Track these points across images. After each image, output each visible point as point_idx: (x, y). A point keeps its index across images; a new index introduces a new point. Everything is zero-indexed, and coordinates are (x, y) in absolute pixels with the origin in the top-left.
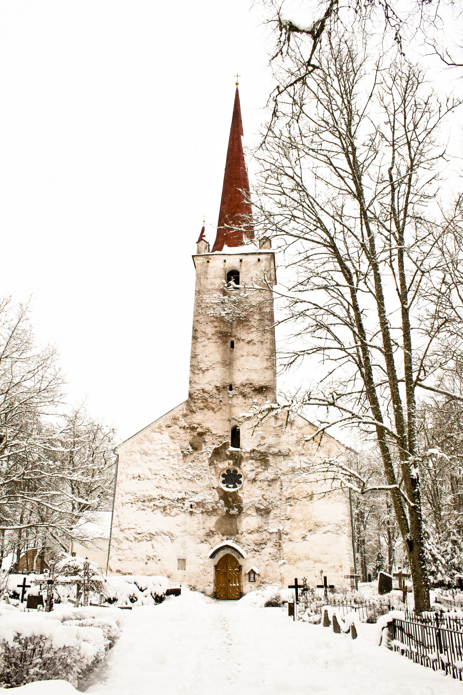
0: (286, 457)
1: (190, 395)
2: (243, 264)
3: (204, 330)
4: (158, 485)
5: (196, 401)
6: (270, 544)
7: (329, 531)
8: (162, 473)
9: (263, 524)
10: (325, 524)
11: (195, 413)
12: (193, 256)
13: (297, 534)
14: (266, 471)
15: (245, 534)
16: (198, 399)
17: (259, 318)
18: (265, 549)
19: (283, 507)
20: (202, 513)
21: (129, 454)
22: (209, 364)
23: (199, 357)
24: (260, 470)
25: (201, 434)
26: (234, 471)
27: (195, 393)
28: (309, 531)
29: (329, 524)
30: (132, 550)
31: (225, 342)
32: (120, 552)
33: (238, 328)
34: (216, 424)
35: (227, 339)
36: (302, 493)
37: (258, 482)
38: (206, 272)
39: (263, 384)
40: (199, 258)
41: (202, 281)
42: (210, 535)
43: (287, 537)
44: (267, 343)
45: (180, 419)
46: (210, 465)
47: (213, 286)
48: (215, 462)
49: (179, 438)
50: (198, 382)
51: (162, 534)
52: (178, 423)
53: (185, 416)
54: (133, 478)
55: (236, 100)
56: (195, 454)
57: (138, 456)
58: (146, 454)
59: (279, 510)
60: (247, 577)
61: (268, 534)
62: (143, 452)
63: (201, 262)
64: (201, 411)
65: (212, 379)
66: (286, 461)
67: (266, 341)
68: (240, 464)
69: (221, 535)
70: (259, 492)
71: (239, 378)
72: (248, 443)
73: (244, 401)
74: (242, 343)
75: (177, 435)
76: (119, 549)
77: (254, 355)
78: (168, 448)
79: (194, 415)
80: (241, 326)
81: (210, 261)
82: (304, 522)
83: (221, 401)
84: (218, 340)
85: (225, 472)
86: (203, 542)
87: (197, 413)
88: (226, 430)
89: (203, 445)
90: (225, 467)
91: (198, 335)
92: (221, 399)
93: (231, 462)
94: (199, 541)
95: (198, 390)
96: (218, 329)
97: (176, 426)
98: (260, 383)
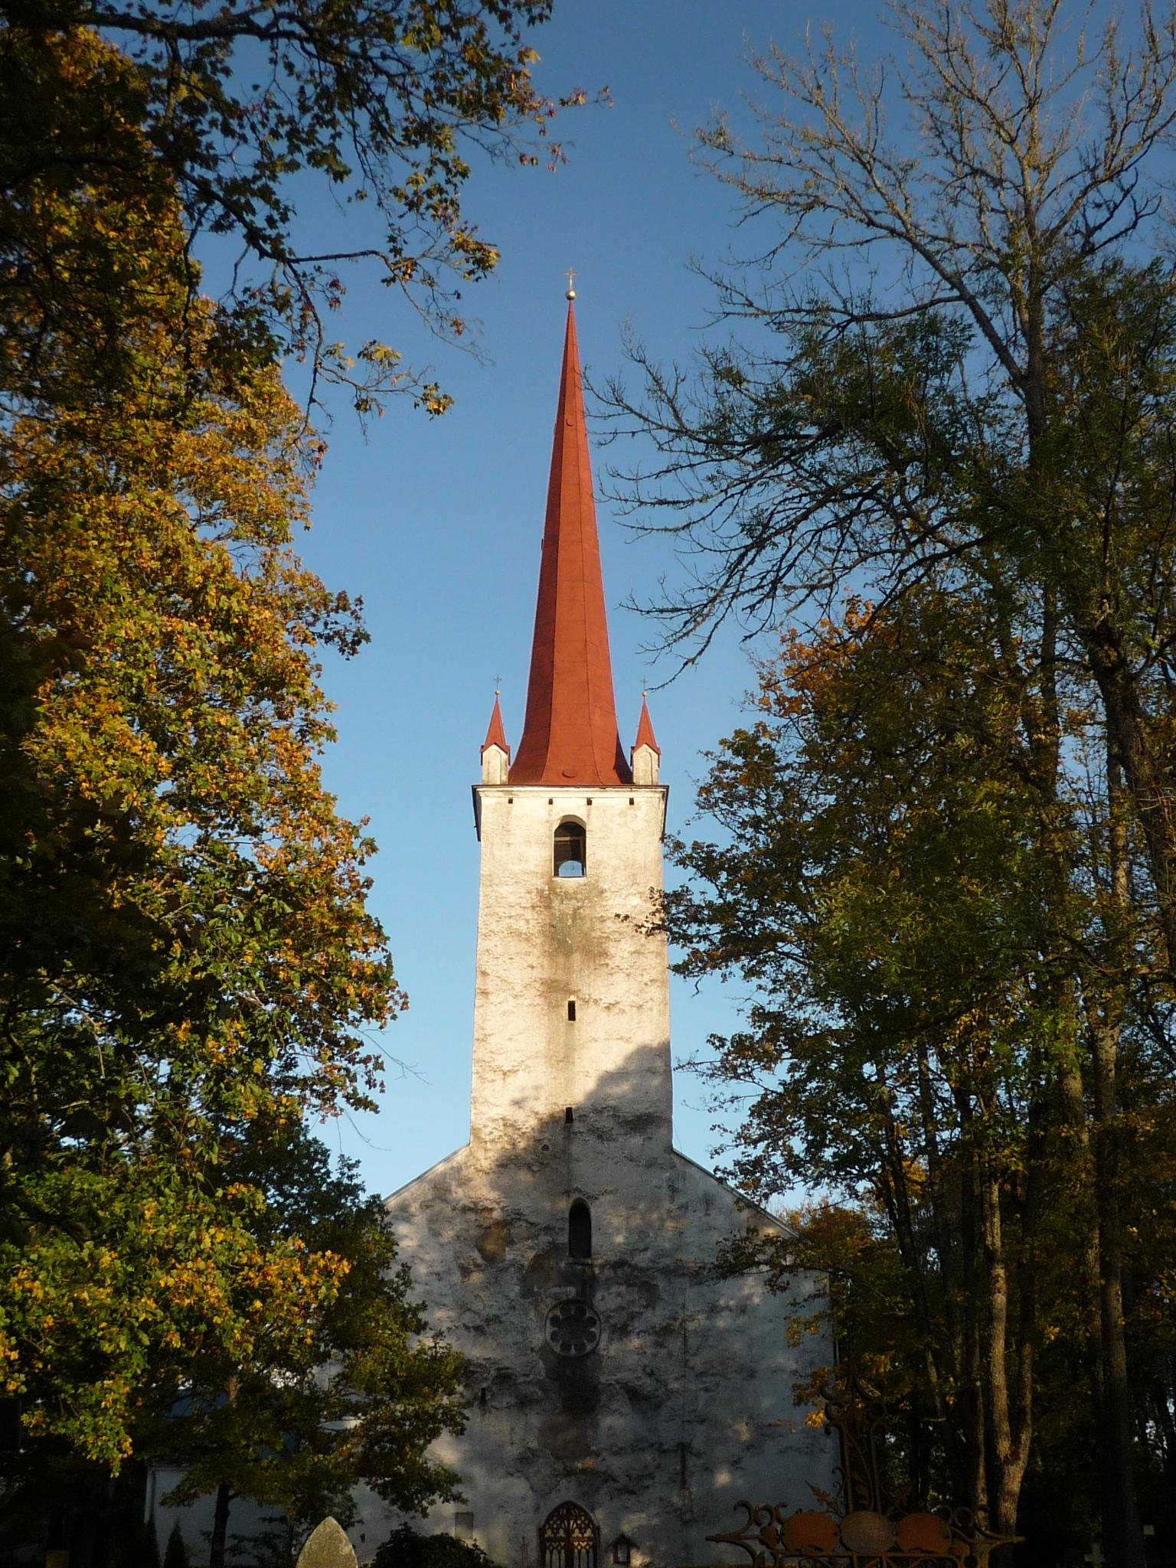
3: (502, 973)
7: (791, 1448)
12: (667, 787)
17: (632, 949)
31: (553, 1007)
39: (641, 1109)
41: (496, 852)
43: (699, 1462)
44: (651, 1009)
46: (523, 1296)
50: (493, 1101)
77: (621, 1038)
95: (494, 1120)
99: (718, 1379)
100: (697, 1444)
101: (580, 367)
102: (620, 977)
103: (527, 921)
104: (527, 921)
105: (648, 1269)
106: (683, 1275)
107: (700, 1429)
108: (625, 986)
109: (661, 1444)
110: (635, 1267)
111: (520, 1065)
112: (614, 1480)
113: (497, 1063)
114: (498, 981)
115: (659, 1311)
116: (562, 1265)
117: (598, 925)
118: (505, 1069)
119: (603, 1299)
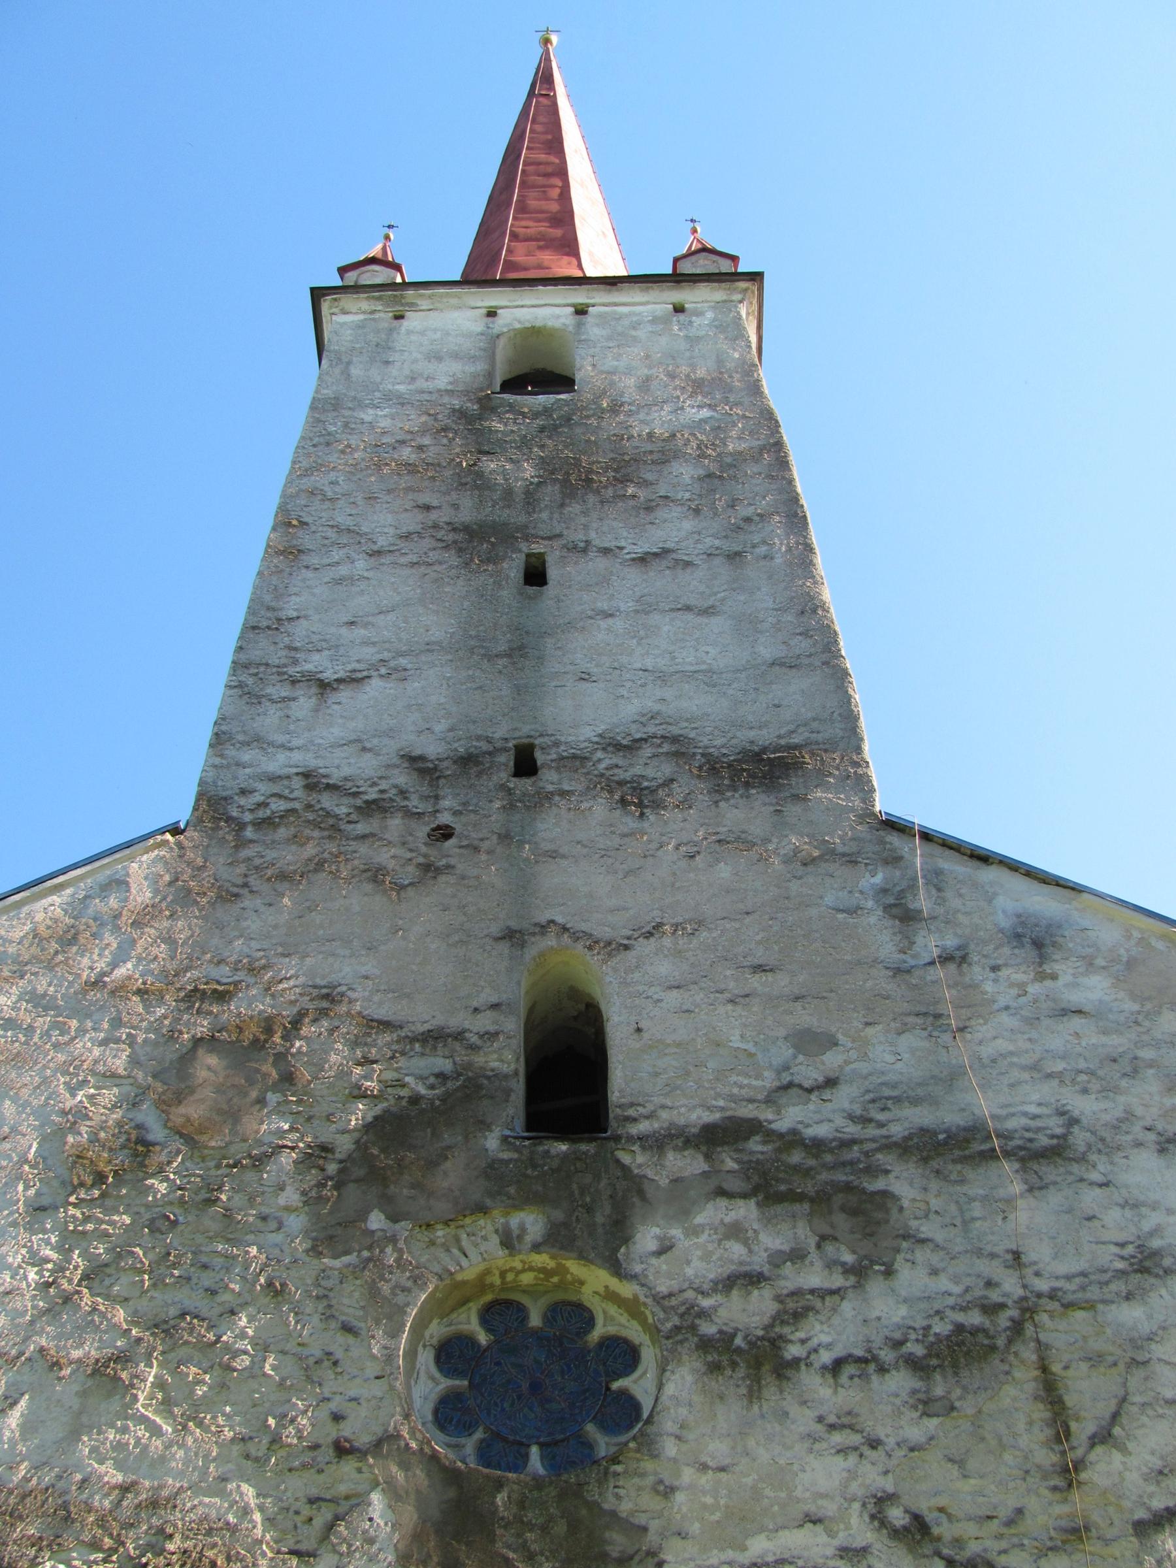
0: (1050, 1172)
12: (318, 294)
14: (876, 1286)
24: (814, 1277)
26: (555, 1311)
37: (813, 1383)
39: (765, 737)
40: (347, 301)
50: (280, 738)
66: (1055, 1199)
70: (824, 1474)
71: (581, 711)
72: (674, 1051)
77: (688, 608)
83: (444, 833)
84: (433, 556)
85: (470, 1323)
88: (488, 996)
91: (305, 539)
92: (445, 818)
93: (531, 1222)
95: (273, 778)
96: (443, 516)
98: (752, 734)
108: (688, 525)
110: (792, 1140)
113: (309, 667)
114: (331, 533)
116: (492, 1142)
118: (329, 675)
119: (665, 1249)
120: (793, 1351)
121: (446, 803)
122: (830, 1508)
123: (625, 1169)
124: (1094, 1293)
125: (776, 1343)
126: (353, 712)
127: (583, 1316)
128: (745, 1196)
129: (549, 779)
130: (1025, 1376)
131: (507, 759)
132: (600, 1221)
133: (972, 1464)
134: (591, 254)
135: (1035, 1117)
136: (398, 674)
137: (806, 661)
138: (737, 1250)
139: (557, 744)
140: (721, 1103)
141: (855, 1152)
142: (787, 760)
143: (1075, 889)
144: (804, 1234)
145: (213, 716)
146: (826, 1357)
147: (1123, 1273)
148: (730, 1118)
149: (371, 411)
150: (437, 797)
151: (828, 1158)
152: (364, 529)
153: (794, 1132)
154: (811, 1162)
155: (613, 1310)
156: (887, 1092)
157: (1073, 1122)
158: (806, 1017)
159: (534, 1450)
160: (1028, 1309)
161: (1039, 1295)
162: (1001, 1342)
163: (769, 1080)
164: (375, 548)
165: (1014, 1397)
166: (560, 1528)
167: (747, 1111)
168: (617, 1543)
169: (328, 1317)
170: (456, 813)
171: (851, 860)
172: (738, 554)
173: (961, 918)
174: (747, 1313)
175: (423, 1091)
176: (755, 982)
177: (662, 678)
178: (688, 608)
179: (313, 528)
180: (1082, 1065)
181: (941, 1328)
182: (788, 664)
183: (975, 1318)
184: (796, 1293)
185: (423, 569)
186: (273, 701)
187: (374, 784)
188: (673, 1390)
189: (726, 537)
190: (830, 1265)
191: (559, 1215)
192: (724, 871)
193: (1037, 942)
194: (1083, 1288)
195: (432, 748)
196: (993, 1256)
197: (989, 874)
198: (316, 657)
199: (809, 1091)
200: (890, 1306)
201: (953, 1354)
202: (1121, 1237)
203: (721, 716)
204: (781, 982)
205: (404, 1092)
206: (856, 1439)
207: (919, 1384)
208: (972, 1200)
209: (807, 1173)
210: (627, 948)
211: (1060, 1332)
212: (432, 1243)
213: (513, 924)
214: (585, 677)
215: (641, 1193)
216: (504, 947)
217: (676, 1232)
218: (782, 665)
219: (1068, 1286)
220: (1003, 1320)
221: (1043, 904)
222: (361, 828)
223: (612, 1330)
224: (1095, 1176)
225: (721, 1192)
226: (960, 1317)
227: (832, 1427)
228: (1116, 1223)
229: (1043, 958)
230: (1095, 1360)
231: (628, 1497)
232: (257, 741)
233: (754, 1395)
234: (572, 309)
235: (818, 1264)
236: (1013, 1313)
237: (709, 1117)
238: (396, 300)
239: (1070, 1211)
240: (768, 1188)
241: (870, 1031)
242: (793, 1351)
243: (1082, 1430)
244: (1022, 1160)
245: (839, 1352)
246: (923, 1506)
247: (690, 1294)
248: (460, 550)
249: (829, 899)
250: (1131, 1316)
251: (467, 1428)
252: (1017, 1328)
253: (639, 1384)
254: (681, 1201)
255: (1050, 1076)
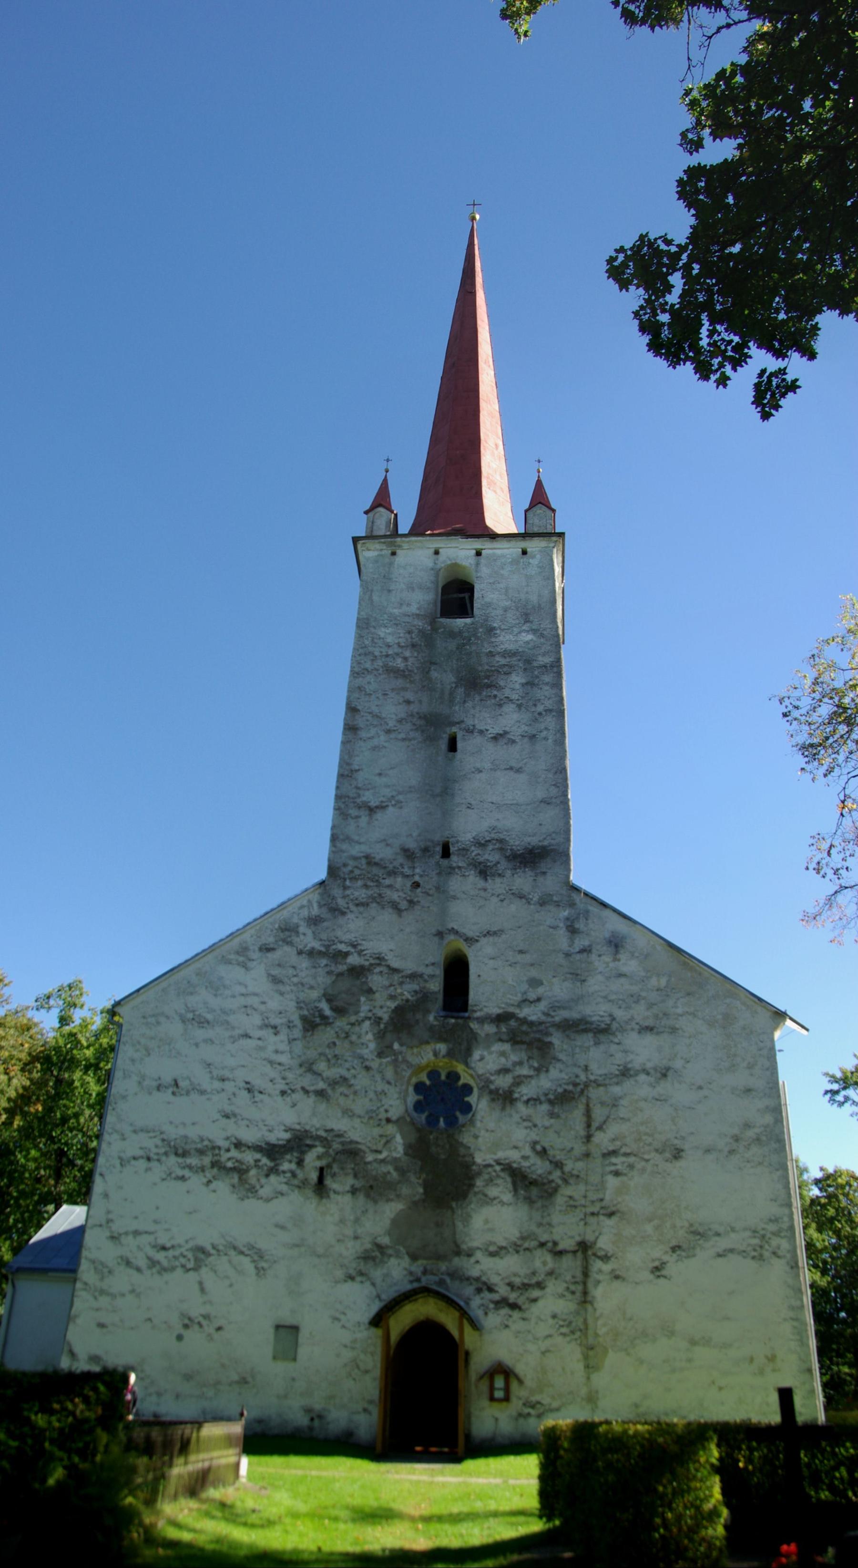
0: (602, 1037)
1: (332, 870)
2: (482, 560)
3: (375, 710)
4: (228, 1109)
5: (348, 883)
6: (553, 1287)
7: (731, 1251)
8: (241, 1075)
9: (533, 1228)
10: (721, 1230)
11: (343, 914)
12: (355, 540)
13: (636, 1258)
14: (543, 1075)
15: (479, 1255)
16: (354, 879)
17: (524, 681)
18: (540, 1303)
19: (594, 1179)
20: (354, 1191)
21: (152, 1020)
22: (387, 792)
23: (361, 777)
24: (525, 1071)
25: (357, 972)
27: (345, 865)
28: (674, 1249)
29: (733, 1230)
30: (138, 1295)
31: (431, 739)
32: (104, 1301)
33: (469, 704)
34: (399, 944)
35: (442, 736)
36: (650, 1140)
37: (520, 1106)
38: (387, 578)
39: (534, 841)
40: (371, 544)
41: (375, 598)
42: (374, 1259)
43: (607, 1267)
44: (546, 739)
45: (302, 929)
46: (380, 1055)
47: (405, 609)
48: (396, 1046)
49: (295, 980)
50: (356, 838)
51: (232, 1253)
52: (296, 940)
53: (314, 921)
54: (158, 1088)
55: (468, 246)
56: (341, 1023)
57: (175, 1029)
58: (203, 1023)
59: (582, 1187)
60: (484, 1386)
61: (549, 1258)
62: (190, 1016)
63: (376, 553)
64: (361, 909)
65: (393, 829)
66: (602, 1047)
67: (544, 733)
68: (468, 1052)
69: (407, 1259)
70: (521, 1134)
71: (468, 826)
72: (489, 988)
73: (481, 883)
74: (477, 740)
75: (291, 972)
76: (102, 1292)
77: (511, 768)
78: (262, 1008)
79: (341, 920)
80: (477, 698)
81: (399, 552)
82: (656, 1222)
83: (416, 885)
84: (412, 734)
85: (424, 1078)
86: (352, 1278)
87: (350, 916)
88: (431, 959)
89: (363, 999)
90: (424, 1062)
91: (360, 722)
92: (417, 878)
93: (442, 1047)
94: (339, 1273)
95: (355, 858)
96: (414, 708)
97: (287, 948)
98: (529, 839)
99: (632, 1159)
100: (604, 1243)
101: (302, 1420)
102: (509, 708)
103: (406, 659)
104: (406, 659)
105: (541, 1023)
106: (585, 1031)
107: (609, 1223)
108: (516, 716)
109: (555, 1244)
110: (524, 1021)
111: (390, 800)
112: (490, 1290)
113: (364, 799)
114: (369, 717)
115: (554, 1073)
116: (431, 1018)
117: (485, 660)
118: (373, 804)
119: (482, 1059)
120: (516, 1095)
121: (417, 871)
122: (520, 1144)
123: (471, 1029)
124: (607, 1082)
125: (511, 1092)
126: (387, 819)
127: (458, 1077)
128: (507, 1041)
129: (455, 860)
130: (581, 1107)
131: (439, 849)
132: (462, 1045)
133: (562, 1134)
134: (488, 478)
135: (602, 1016)
136: (399, 804)
137: (554, 800)
138: (503, 1060)
139: (458, 842)
140: (503, 1006)
141: (542, 1027)
142: (544, 855)
143: (635, 922)
144: (524, 1056)
145: (330, 825)
146: (525, 1098)
147: (617, 1075)
148: (505, 1012)
149: (383, 629)
150: (414, 868)
151: (535, 1028)
152: (384, 716)
153: (525, 1018)
154: (529, 1030)
155: (466, 1075)
156: (557, 1004)
157: (614, 1019)
158: (534, 973)
159: (442, 1120)
160: (587, 1085)
161: (591, 1081)
162: (576, 1096)
163: (519, 998)
164: (388, 728)
165: (577, 1115)
166: (447, 1146)
167: (511, 1010)
168: (462, 1151)
169: (383, 1079)
170: (421, 876)
171: (558, 904)
172: (534, 736)
173: (593, 933)
174: (503, 1082)
175: (410, 997)
176: (519, 958)
177: (499, 807)
178: (511, 768)
179: (362, 714)
180: (621, 997)
181: (560, 1090)
182: (546, 802)
183: (570, 1088)
184: (519, 1076)
185: (407, 743)
186: (352, 818)
187: (391, 863)
188: (480, 1103)
189: (530, 725)
190: (531, 1067)
191: (451, 1046)
192: (513, 908)
193: (616, 944)
194: (604, 1079)
195: (412, 845)
196: (579, 1067)
197: (607, 913)
198: (367, 793)
199: (531, 1002)
200: (545, 1083)
201: (562, 1099)
202: (619, 1062)
203: (521, 830)
204: (527, 958)
205: (404, 998)
206: (530, 1124)
207: (551, 1108)
208: (576, 1046)
209: (526, 1033)
210: (477, 941)
211: (594, 1093)
212: (413, 1054)
213: (440, 929)
214: (470, 807)
215: (476, 1039)
216: (436, 939)
217: (485, 1053)
218: (545, 802)
219: (600, 1079)
220: (579, 1089)
221: (621, 927)
222: (387, 882)
223: (466, 1081)
224: (616, 1040)
225: (501, 1040)
226: (566, 1087)
227: (524, 1120)
228: (619, 1058)
229: (617, 952)
230: (603, 1104)
231: (466, 1138)
232: (348, 839)
233: (503, 1109)
234: (474, 552)
235: (527, 1067)
236: (582, 1086)
237: (499, 1011)
238: (393, 544)
239: (606, 1053)
240: (514, 1039)
241: (554, 980)
242: (516, 1095)
243: (595, 1125)
244: (595, 1033)
245: (529, 1096)
246: (546, 1145)
247: (488, 1075)
248: (423, 731)
249: (548, 923)
250: (616, 1090)
251: (422, 1111)
252: (582, 1092)
253: (472, 1099)
254: (489, 1040)
255: (610, 1001)
